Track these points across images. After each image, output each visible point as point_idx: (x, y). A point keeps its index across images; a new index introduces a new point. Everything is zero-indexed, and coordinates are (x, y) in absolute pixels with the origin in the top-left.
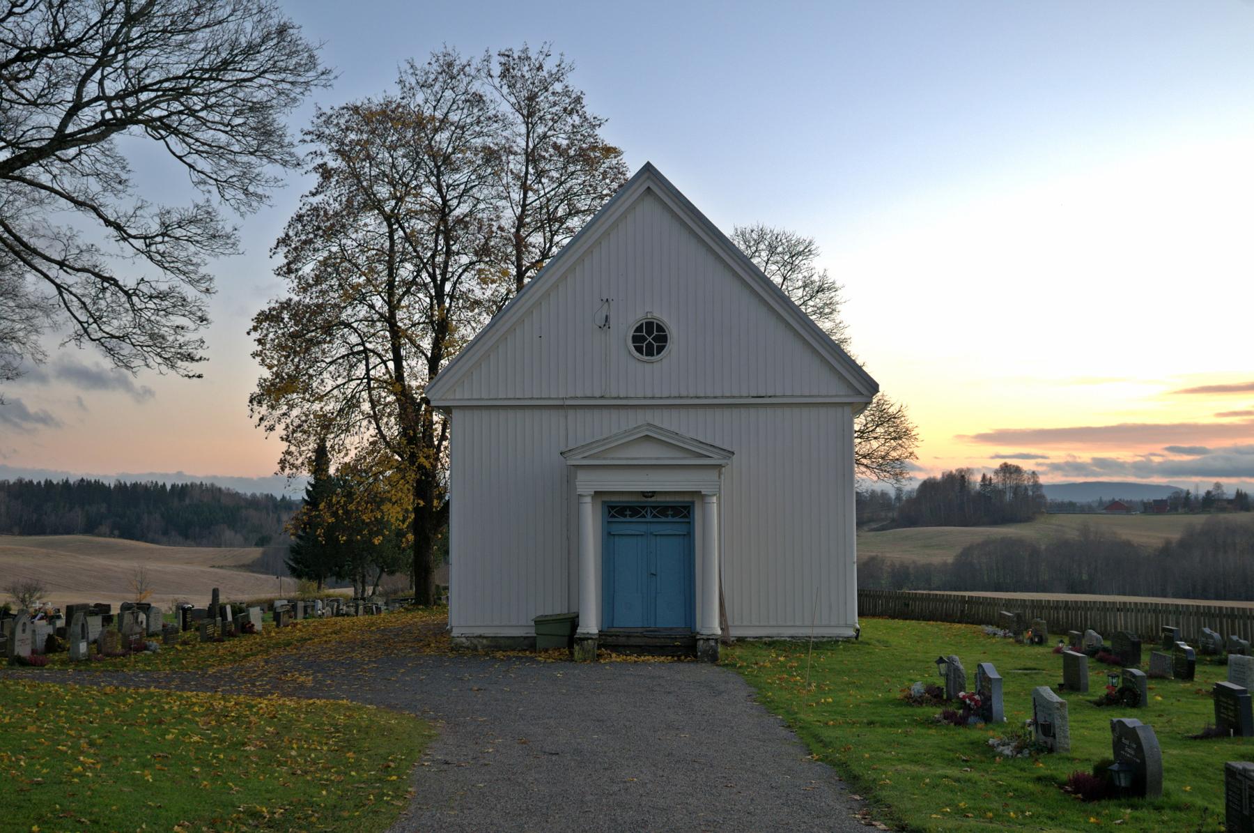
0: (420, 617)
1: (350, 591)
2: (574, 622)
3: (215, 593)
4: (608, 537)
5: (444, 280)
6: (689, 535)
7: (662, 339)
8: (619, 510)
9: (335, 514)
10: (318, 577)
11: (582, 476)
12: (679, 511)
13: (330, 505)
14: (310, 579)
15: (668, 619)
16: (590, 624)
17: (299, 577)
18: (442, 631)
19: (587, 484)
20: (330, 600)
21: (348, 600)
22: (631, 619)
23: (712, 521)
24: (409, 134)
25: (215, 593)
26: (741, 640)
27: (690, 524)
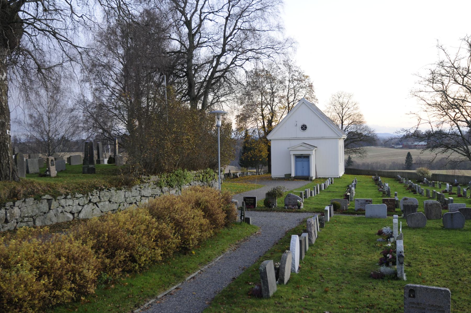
0: (268, 175)
1: (255, 170)
2: (290, 175)
3: (230, 171)
4: (296, 161)
5: (127, 102)
6: (309, 161)
7: (306, 128)
8: (298, 157)
9: (252, 155)
10: (247, 166)
11: (291, 152)
12: (307, 157)
13: (251, 153)
14: (245, 167)
15: (305, 174)
16: (293, 175)
17: (242, 167)
18: (271, 177)
19: (292, 153)
20: (251, 172)
21: (255, 172)
22: (300, 174)
23: (313, 160)
24: (185, 70)
25: (230, 171)
26: (320, 178)
27: (309, 159)
